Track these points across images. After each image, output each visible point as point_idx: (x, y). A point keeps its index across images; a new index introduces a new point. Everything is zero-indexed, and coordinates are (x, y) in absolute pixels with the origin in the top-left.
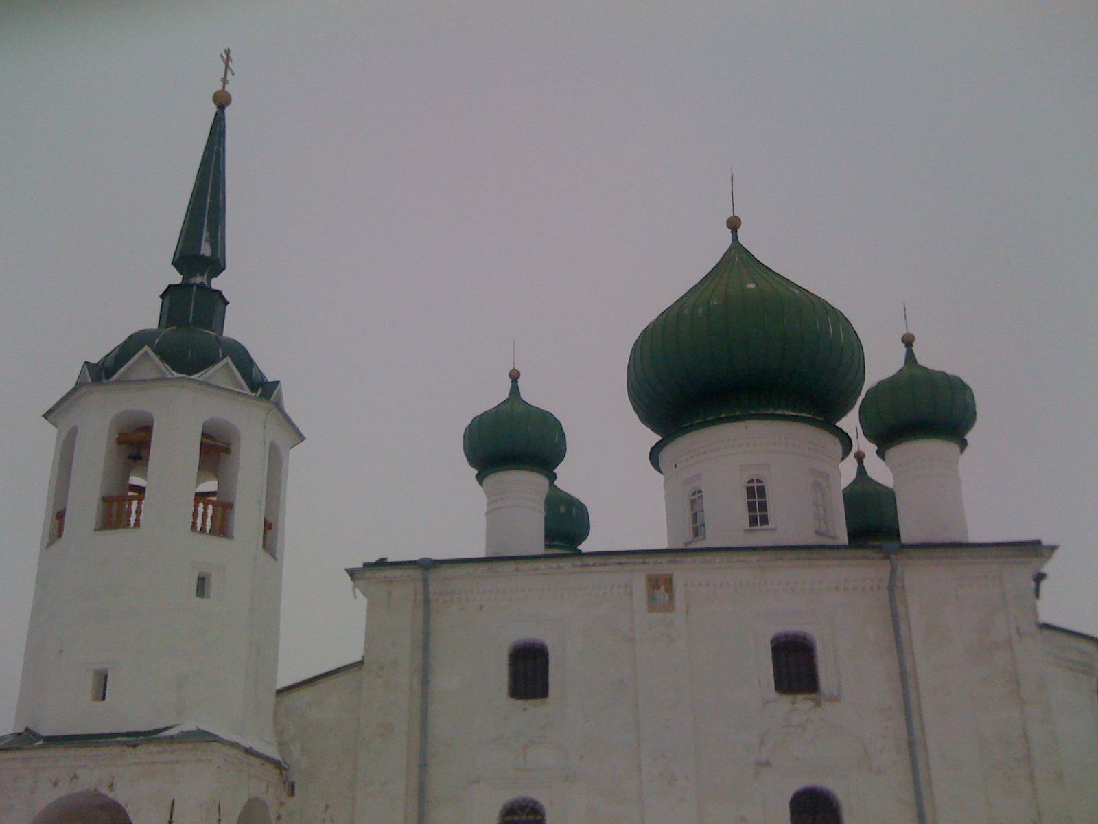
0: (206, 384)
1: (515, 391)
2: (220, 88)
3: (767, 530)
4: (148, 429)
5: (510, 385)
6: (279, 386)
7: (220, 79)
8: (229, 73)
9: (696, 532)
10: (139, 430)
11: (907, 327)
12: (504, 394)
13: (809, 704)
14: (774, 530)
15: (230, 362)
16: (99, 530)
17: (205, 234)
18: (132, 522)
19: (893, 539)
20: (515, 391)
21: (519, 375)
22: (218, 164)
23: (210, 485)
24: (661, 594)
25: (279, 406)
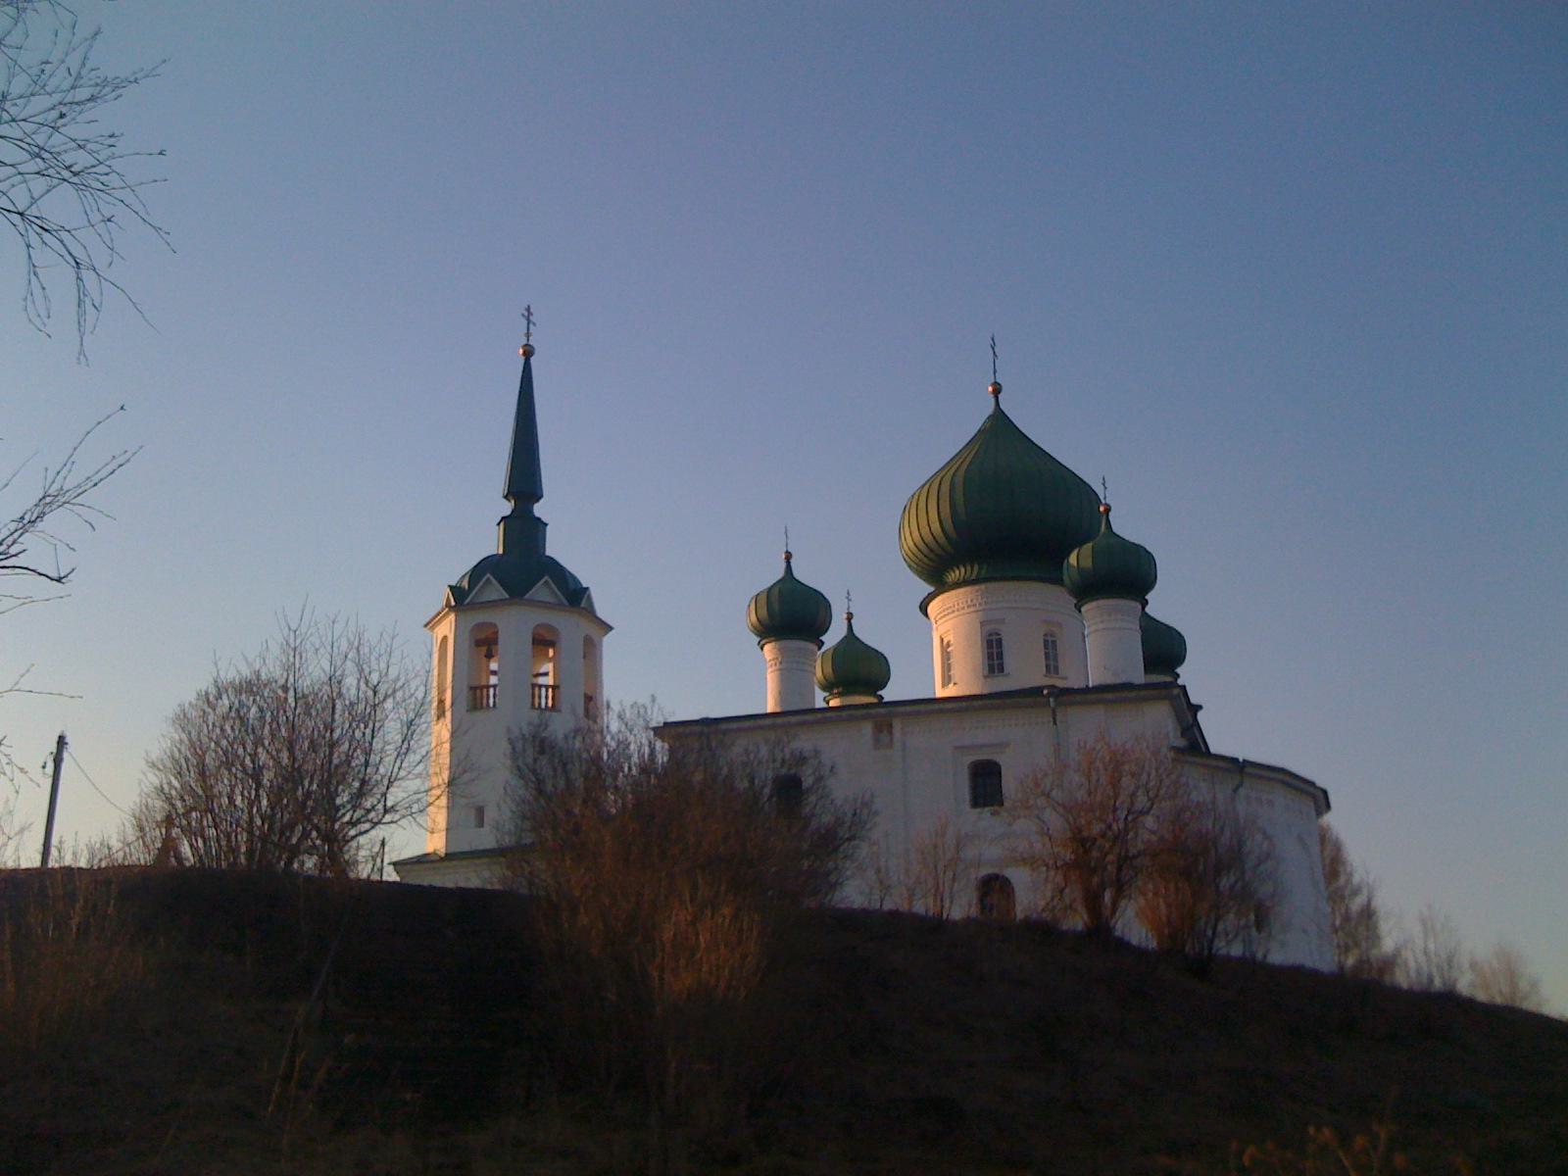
8: (531, 326)
12: (780, 573)
15: (491, 578)
18: (491, 704)
24: (884, 737)
25: (590, 612)
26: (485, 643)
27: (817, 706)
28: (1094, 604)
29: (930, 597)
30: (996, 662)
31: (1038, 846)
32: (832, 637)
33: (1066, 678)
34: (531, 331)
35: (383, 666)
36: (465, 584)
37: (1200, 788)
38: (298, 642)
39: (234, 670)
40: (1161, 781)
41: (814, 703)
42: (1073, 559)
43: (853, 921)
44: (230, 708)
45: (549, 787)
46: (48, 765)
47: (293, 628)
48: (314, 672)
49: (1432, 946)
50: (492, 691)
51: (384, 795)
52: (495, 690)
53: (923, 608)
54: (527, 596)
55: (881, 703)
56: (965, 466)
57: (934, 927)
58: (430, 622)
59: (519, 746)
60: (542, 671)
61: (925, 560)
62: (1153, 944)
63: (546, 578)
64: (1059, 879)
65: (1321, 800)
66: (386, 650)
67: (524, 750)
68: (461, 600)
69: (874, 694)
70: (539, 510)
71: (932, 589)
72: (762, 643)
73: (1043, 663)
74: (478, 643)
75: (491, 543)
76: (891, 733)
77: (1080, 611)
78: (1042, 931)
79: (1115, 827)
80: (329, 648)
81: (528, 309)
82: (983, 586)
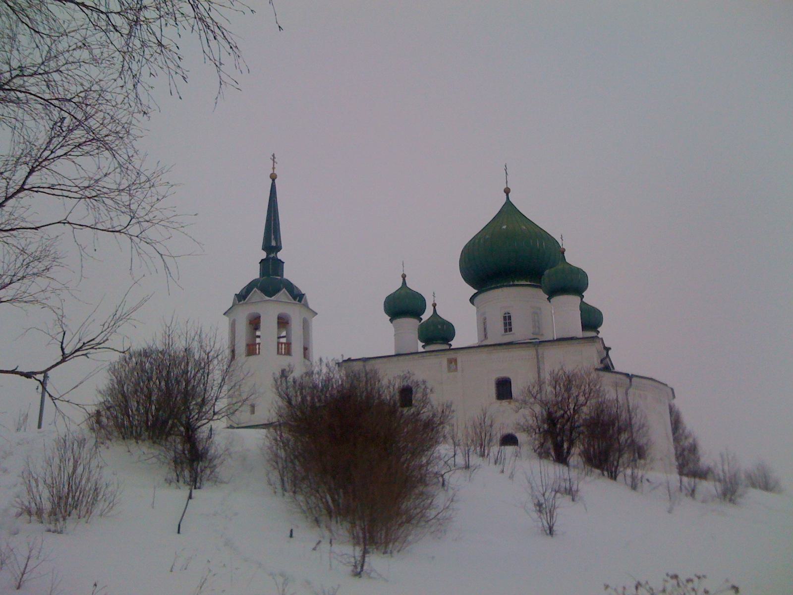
0: (277, 301)
1: (404, 283)
2: (272, 172)
3: (511, 334)
4: (260, 317)
5: (402, 280)
6: (304, 297)
8: (275, 164)
9: (486, 336)
10: (255, 319)
12: (400, 285)
13: (507, 403)
14: (514, 334)
17: (273, 237)
18: (257, 352)
20: (404, 283)
21: (405, 276)
22: (275, 220)
23: (284, 334)
25: (306, 306)
27: (419, 351)
31: (531, 422)
32: (426, 316)
34: (275, 166)
35: (212, 344)
38: (171, 332)
40: (591, 389)
41: (418, 349)
44: (136, 363)
45: (293, 402)
46: (39, 388)
47: (168, 325)
48: (180, 345)
49: (726, 468)
50: (258, 346)
51: (214, 405)
52: (259, 346)
66: (213, 335)
67: (281, 384)
70: (280, 255)
71: (476, 291)
79: (568, 413)
80: (185, 335)
81: (273, 155)
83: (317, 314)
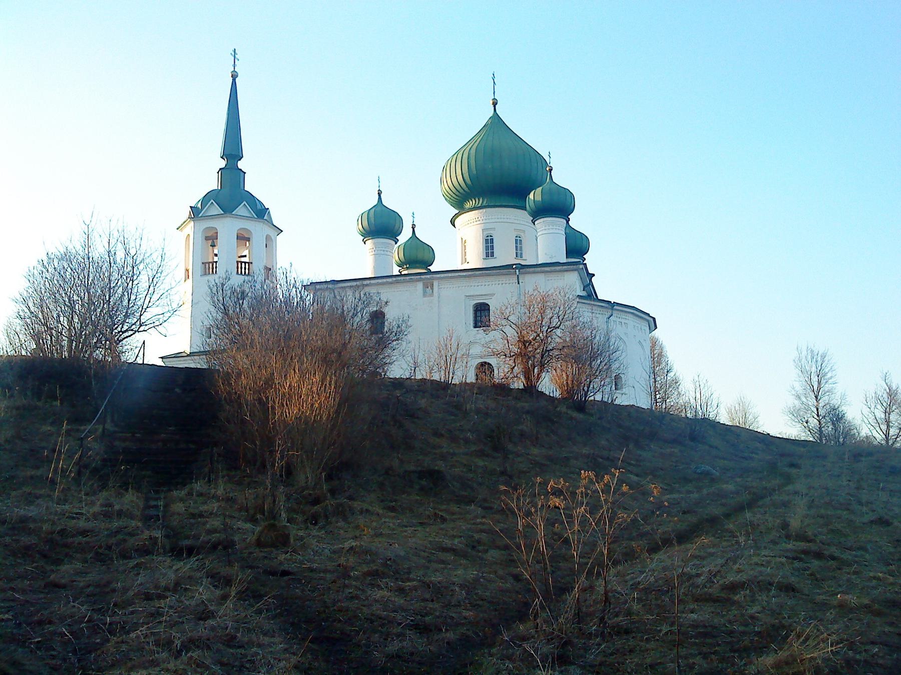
7: (237, 65)
8: (236, 60)
11: (136, 357)
15: (214, 202)
16: (203, 275)
19: (672, 420)
24: (429, 290)
26: (212, 239)
28: (542, 220)
29: (456, 216)
30: (490, 251)
33: (526, 260)
36: (199, 205)
37: (586, 313)
39: (56, 248)
42: (531, 196)
43: (398, 383)
52: (216, 264)
53: (453, 223)
54: (233, 213)
55: (430, 272)
56: (476, 145)
57: (444, 387)
58: (179, 227)
59: (214, 289)
60: (243, 254)
61: (454, 195)
62: (557, 394)
63: (245, 202)
64: (511, 362)
65: (653, 324)
68: (195, 213)
69: (426, 269)
70: (241, 165)
72: (365, 240)
73: (495, 251)
74: (207, 238)
75: (213, 183)
76: (432, 289)
77: (534, 224)
78: (502, 389)
82: (484, 210)
83: (282, 231)
